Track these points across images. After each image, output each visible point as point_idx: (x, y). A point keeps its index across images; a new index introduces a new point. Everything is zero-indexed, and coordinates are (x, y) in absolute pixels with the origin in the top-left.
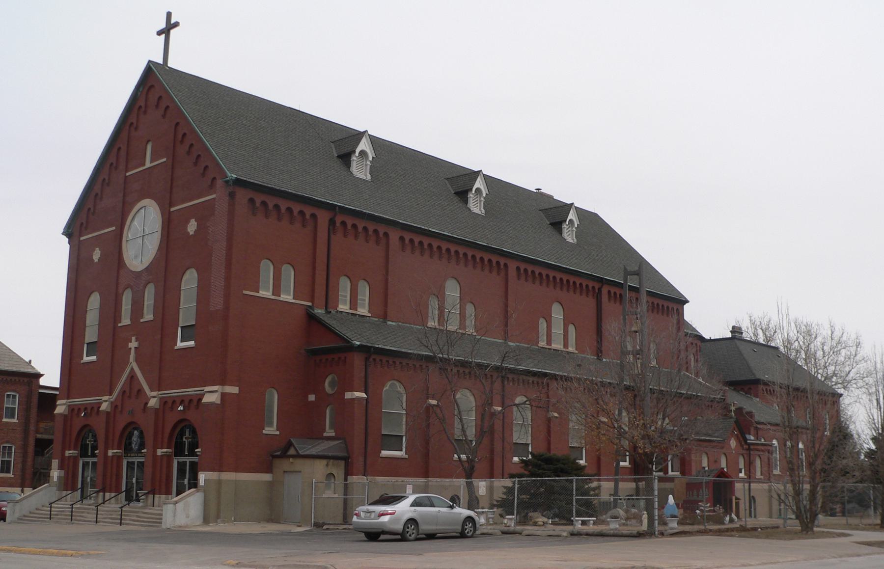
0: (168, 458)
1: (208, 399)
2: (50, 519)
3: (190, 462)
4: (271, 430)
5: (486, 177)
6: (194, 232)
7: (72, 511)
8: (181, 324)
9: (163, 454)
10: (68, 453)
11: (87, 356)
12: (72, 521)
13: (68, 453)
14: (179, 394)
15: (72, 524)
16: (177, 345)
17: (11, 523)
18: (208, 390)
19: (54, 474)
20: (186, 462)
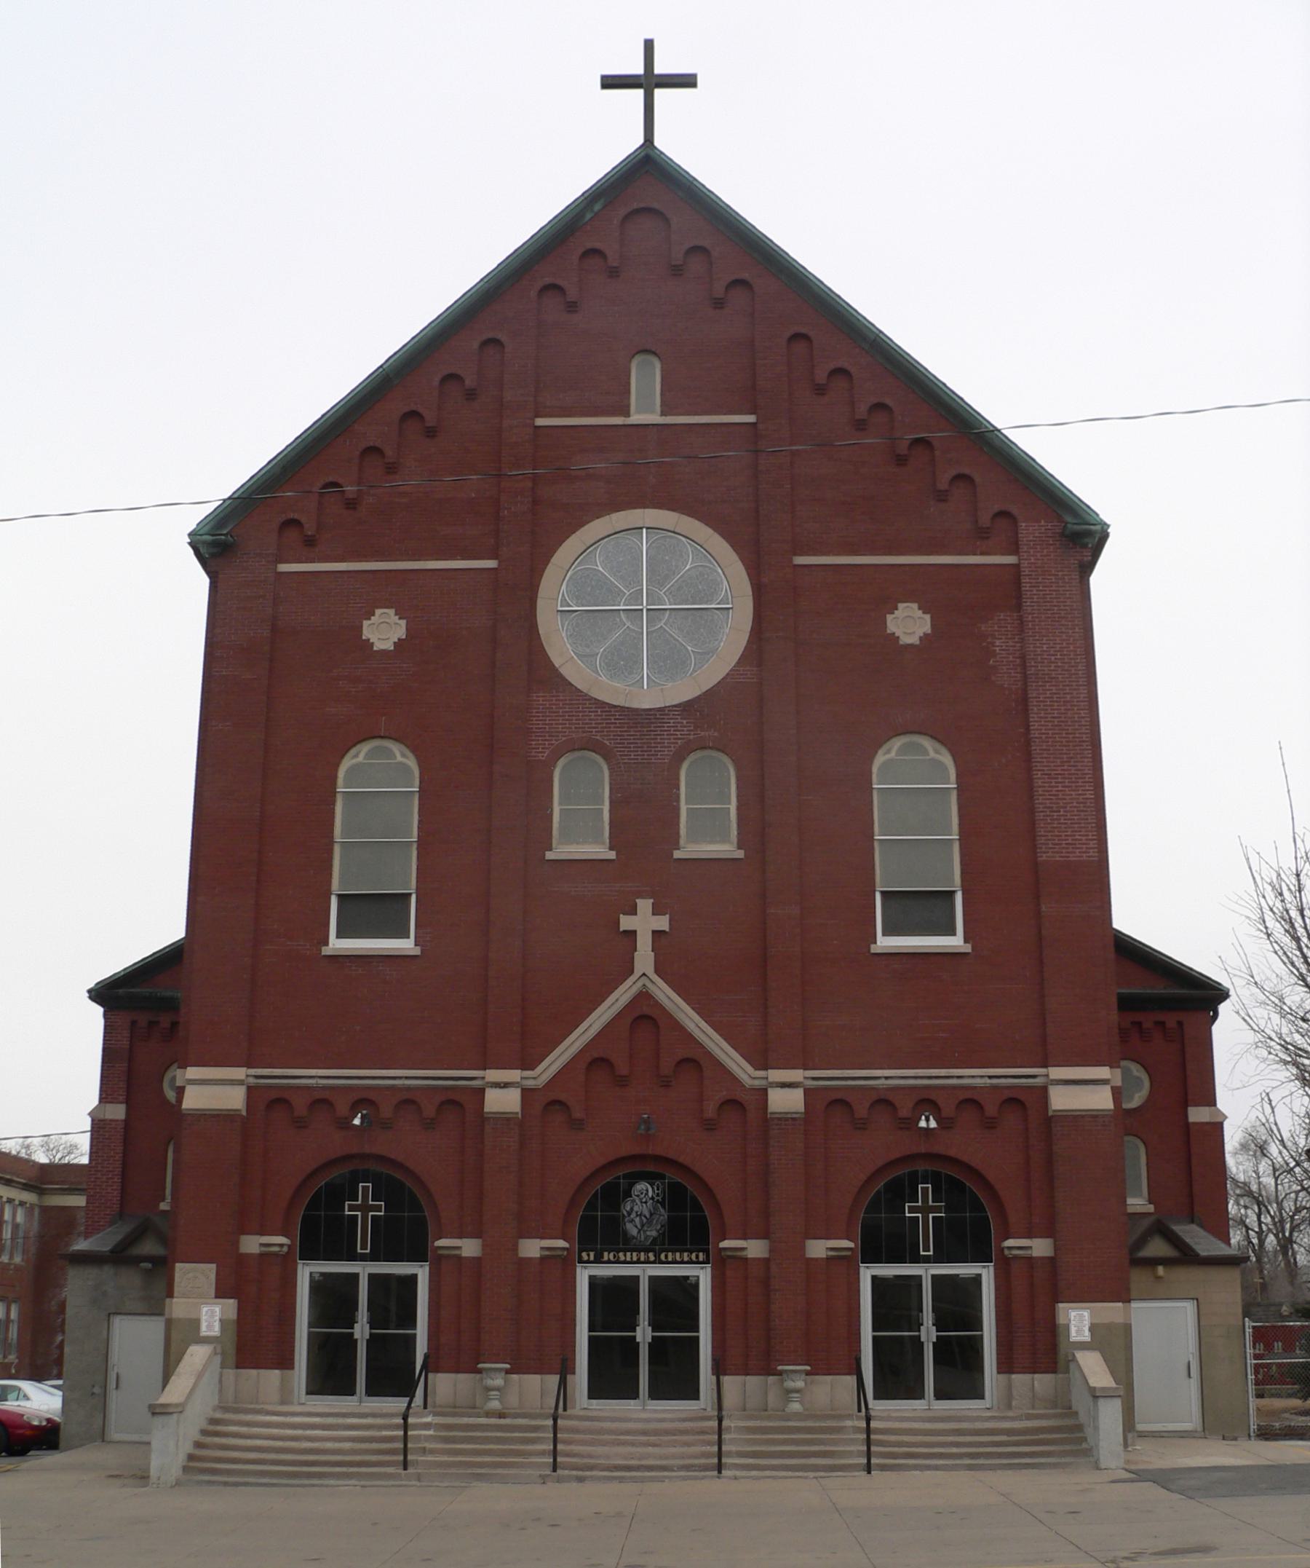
0: (844, 1266)
1: (1061, 1100)
2: (405, 1468)
3: (373, 1278)
4: (1138, 1202)
5: (641, 680)
6: (921, 638)
7: (868, 1430)
8: (879, 888)
9: (547, 1253)
10: (251, 1244)
11: (340, 935)
12: (555, 1470)
13: (251, 1244)
14: (995, 1081)
15: (560, 1480)
16: (875, 943)
17: (174, 1486)
18: (778, 1080)
19: (1067, 1315)
20: (356, 1276)
